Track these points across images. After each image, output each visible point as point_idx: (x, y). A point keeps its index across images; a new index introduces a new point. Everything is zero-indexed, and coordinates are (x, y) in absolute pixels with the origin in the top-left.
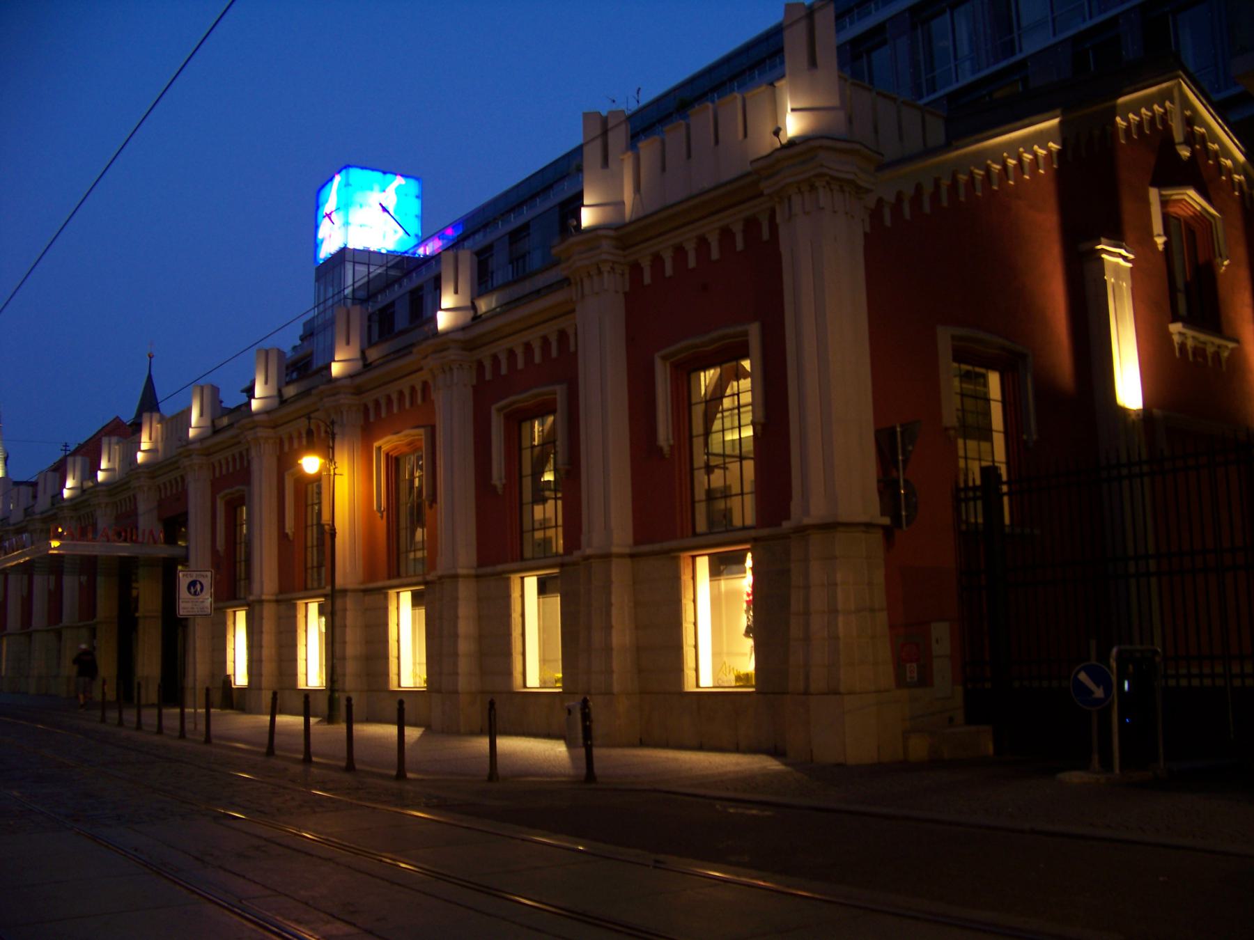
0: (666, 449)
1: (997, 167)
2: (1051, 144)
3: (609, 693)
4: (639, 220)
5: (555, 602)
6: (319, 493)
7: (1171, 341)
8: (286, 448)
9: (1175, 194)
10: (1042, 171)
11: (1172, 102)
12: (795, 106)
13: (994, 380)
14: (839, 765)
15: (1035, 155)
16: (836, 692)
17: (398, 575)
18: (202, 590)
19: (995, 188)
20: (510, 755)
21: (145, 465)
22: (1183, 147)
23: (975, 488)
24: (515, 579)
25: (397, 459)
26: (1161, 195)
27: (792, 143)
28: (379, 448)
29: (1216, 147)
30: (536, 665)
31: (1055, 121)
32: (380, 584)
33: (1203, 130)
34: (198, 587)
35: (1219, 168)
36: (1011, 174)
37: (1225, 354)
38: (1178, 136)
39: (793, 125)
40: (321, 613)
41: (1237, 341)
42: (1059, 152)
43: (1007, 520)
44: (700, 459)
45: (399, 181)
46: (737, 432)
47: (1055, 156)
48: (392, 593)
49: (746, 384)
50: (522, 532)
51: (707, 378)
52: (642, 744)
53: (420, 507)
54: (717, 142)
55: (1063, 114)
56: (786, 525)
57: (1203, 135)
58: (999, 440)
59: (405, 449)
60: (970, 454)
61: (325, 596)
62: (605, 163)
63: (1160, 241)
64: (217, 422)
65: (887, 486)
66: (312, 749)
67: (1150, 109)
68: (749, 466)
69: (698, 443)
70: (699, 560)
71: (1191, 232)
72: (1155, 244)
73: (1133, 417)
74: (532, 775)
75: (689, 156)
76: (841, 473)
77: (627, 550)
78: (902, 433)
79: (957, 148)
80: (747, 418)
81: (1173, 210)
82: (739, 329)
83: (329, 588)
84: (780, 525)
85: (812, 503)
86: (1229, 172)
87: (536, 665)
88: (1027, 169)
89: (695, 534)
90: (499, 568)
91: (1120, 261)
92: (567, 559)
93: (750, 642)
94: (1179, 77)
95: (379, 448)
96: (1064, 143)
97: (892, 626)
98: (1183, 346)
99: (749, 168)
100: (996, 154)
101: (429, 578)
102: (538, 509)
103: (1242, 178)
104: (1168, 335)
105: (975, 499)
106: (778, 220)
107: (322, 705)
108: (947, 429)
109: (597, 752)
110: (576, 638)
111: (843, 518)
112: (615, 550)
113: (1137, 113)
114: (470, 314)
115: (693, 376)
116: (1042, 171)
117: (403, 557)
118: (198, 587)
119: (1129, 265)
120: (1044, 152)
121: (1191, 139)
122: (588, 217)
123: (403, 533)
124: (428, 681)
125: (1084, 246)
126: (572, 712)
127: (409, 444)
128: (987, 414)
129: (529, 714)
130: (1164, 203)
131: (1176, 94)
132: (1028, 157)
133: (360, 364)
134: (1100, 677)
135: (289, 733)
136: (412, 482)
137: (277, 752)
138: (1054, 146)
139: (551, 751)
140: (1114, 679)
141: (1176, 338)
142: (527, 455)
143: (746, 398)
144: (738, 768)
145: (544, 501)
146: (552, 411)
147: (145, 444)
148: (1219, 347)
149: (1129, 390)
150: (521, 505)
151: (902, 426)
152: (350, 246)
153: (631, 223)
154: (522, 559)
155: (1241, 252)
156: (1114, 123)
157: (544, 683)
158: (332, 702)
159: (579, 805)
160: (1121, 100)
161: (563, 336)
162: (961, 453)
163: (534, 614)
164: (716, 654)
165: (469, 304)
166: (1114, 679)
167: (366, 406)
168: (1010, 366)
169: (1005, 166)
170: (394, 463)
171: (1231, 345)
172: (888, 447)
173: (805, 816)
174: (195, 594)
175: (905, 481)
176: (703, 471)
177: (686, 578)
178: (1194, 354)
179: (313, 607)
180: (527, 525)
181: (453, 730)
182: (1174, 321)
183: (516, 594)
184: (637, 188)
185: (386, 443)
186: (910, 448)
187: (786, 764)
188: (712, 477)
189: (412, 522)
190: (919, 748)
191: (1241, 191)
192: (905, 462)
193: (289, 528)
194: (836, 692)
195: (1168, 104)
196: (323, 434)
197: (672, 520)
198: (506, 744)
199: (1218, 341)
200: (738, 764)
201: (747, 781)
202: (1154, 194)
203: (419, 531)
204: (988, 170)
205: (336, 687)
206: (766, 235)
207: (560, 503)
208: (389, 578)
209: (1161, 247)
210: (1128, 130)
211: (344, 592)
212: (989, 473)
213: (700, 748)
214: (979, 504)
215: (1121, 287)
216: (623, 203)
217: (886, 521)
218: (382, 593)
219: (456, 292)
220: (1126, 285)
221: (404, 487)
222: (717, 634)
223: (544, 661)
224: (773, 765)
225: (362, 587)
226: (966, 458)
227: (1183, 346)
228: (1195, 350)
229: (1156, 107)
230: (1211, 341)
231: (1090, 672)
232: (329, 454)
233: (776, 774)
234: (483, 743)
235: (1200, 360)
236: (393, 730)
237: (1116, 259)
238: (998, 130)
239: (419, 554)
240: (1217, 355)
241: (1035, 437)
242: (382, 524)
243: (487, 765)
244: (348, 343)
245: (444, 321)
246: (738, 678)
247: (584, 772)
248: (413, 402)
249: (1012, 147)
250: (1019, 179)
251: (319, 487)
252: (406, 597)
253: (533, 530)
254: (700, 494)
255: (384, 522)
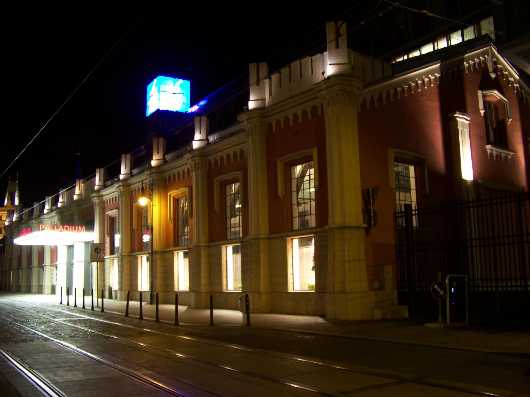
0: (281, 196)
1: (406, 87)
2: (436, 74)
3: (258, 292)
4: (274, 105)
5: (239, 257)
6: (147, 213)
7: (487, 152)
8: (133, 195)
9: (489, 93)
10: (432, 85)
11: (488, 55)
12: (331, 63)
13: (412, 169)
14: (346, 320)
15: (430, 79)
16: (345, 293)
17: (178, 246)
18: (100, 251)
19: (413, 93)
20: (218, 317)
21: (77, 201)
22: (492, 73)
23: (402, 212)
24: (224, 247)
25: (178, 200)
26: (483, 93)
27: (329, 78)
28: (170, 195)
29: (507, 73)
30: (232, 280)
31: (439, 65)
32: (171, 249)
33: (501, 66)
34: (99, 250)
35: (508, 82)
36: (419, 87)
37: (510, 157)
38: (490, 69)
39: (330, 70)
40: (148, 260)
41: (514, 152)
42: (440, 77)
43: (414, 225)
44: (295, 201)
45: (181, 81)
46: (309, 189)
47: (438, 79)
48: (176, 253)
49: (312, 170)
50: (226, 229)
51: (299, 169)
52: (272, 312)
53: (187, 218)
54: (301, 76)
55: (441, 62)
56: (326, 227)
57: (501, 68)
58: (413, 193)
59: (181, 195)
60: (401, 199)
61: (149, 254)
62: (258, 84)
63: (482, 112)
64: (106, 183)
65: (366, 212)
66: (143, 314)
67: (479, 58)
68: (313, 203)
69: (294, 194)
70: (294, 240)
71: (496, 108)
72: (480, 113)
73: (469, 183)
74: (225, 323)
75: (290, 81)
76: (348, 208)
77: (266, 236)
78: (372, 191)
79: (397, 77)
80: (313, 184)
81: (488, 99)
82: (309, 150)
83: (151, 251)
84: (324, 227)
85: (336, 218)
86: (512, 83)
87: (232, 280)
88: (426, 84)
89: (293, 230)
90: (217, 243)
91: (464, 121)
92: (243, 239)
93: (313, 273)
94: (490, 45)
95: (170, 195)
96: (442, 74)
97: (368, 267)
98: (491, 154)
99: (312, 87)
100: (413, 79)
101: (190, 247)
102: (233, 220)
103: (518, 85)
104: (485, 150)
105: (402, 217)
106: (324, 108)
107: (148, 297)
108: (391, 189)
109: (251, 315)
110: (247, 271)
111: (347, 225)
112: (262, 236)
113: (473, 60)
114: (206, 142)
115: (292, 168)
116: (432, 85)
117: (180, 238)
118: (99, 250)
119: (468, 122)
120: (433, 78)
121: (496, 70)
122: (251, 105)
123: (180, 228)
124: (190, 288)
125: (450, 115)
126: (243, 301)
127: (182, 193)
128: (409, 181)
129: (177, 299)
130: (484, 96)
131: (490, 52)
132: (426, 80)
133: (163, 161)
134: (442, 286)
135: (134, 308)
136: (183, 209)
137: (129, 315)
138: (438, 75)
139: (237, 315)
140: (448, 288)
141: (489, 151)
142: (228, 198)
143: (312, 177)
144: (307, 321)
145: (235, 216)
146: (238, 181)
147: (77, 191)
148: (507, 154)
149: (468, 172)
150: (226, 218)
151: (372, 188)
152: (161, 109)
153: (268, 107)
154: (226, 239)
155: (517, 115)
156: (463, 65)
157: (235, 289)
158: (152, 296)
159: (247, 335)
160: (466, 55)
161: (242, 151)
162: (397, 198)
163: (231, 262)
164: (301, 277)
165: (205, 138)
166: (448, 288)
167: (165, 179)
168: (419, 164)
169: (417, 84)
170: (176, 201)
171: (512, 153)
172: (367, 197)
173: (336, 341)
174: (98, 253)
175: (373, 210)
176: (296, 205)
177: (289, 247)
178: (496, 157)
179: (145, 258)
180: (228, 226)
181: (198, 307)
182: (488, 144)
183: (224, 254)
184: (270, 94)
185: (174, 193)
186: (375, 197)
187: (325, 320)
188: (299, 207)
189: (183, 225)
190: (378, 314)
191: (517, 91)
192: (373, 202)
193: (135, 227)
194: (345, 293)
195: (486, 56)
196: (148, 189)
197: (281, 226)
198: (217, 312)
199: (506, 152)
200: (307, 320)
201: (308, 326)
202: (480, 93)
203: (187, 227)
204: (410, 86)
205: (153, 290)
206: (320, 113)
207: (241, 217)
208: (175, 246)
209: (482, 114)
210: (469, 67)
211: (156, 252)
212: (408, 207)
213: (294, 314)
214: (404, 218)
215: (464, 131)
216: (265, 99)
217: (365, 225)
218: (172, 253)
219: (200, 133)
220: (467, 131)
221: (180, 210)
222: (301, 269)
223: (235, 280)
224: (320, 320)
225: (164, 250)
226: (400, 200)
227: (491, 154)
228: (497, 156)
229: (481, 58)
230: (503, 152)
231: (439, 284)
232: (150, 197)
233: (321, 324)
234: (208, 312)
235: (499, 159)
236: (173, 307)
237: (462, 121)
238: (414, 70)
239: (186, 237)
240: (506, 157)
241: (428, 192)
242: (171, 225)
243: (209, 320)
244: (158, 153)
245: (196, 145)
246: (309, 287)
247: (246, 322)
248: (183, 177)
249: (420, 76)
250: (423, 89)
251: (147, 211)
252: (181, 254)
253: (231, 228)
254: (295, 214)
255: (172, 224)
